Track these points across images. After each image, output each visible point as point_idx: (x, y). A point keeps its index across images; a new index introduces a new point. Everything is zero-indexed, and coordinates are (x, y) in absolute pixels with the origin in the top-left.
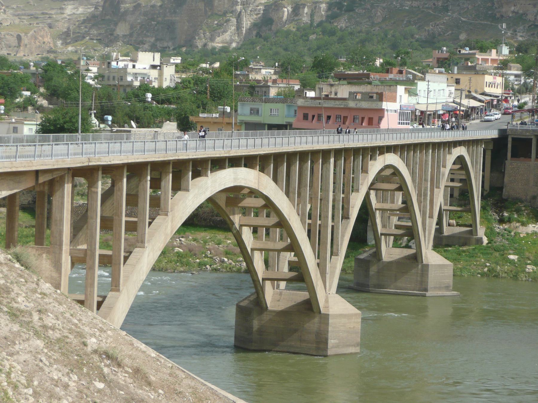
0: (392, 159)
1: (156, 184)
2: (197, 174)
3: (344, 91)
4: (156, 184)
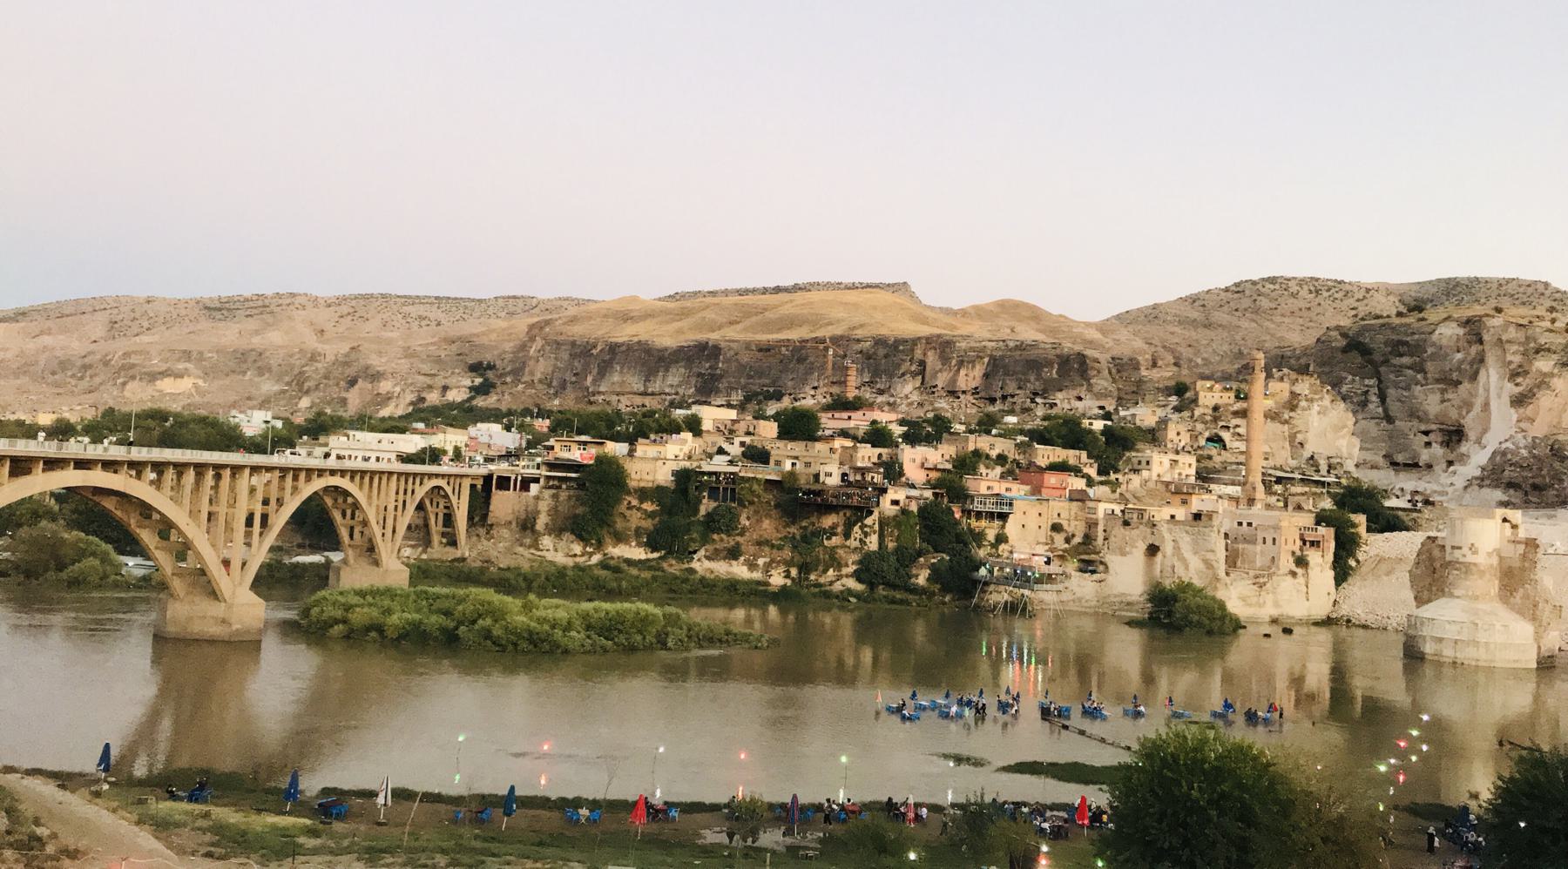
0: (442, 483)
1: (295, 478)
2: (319, 476)
3: (576, 454)
4: (295, 478)
